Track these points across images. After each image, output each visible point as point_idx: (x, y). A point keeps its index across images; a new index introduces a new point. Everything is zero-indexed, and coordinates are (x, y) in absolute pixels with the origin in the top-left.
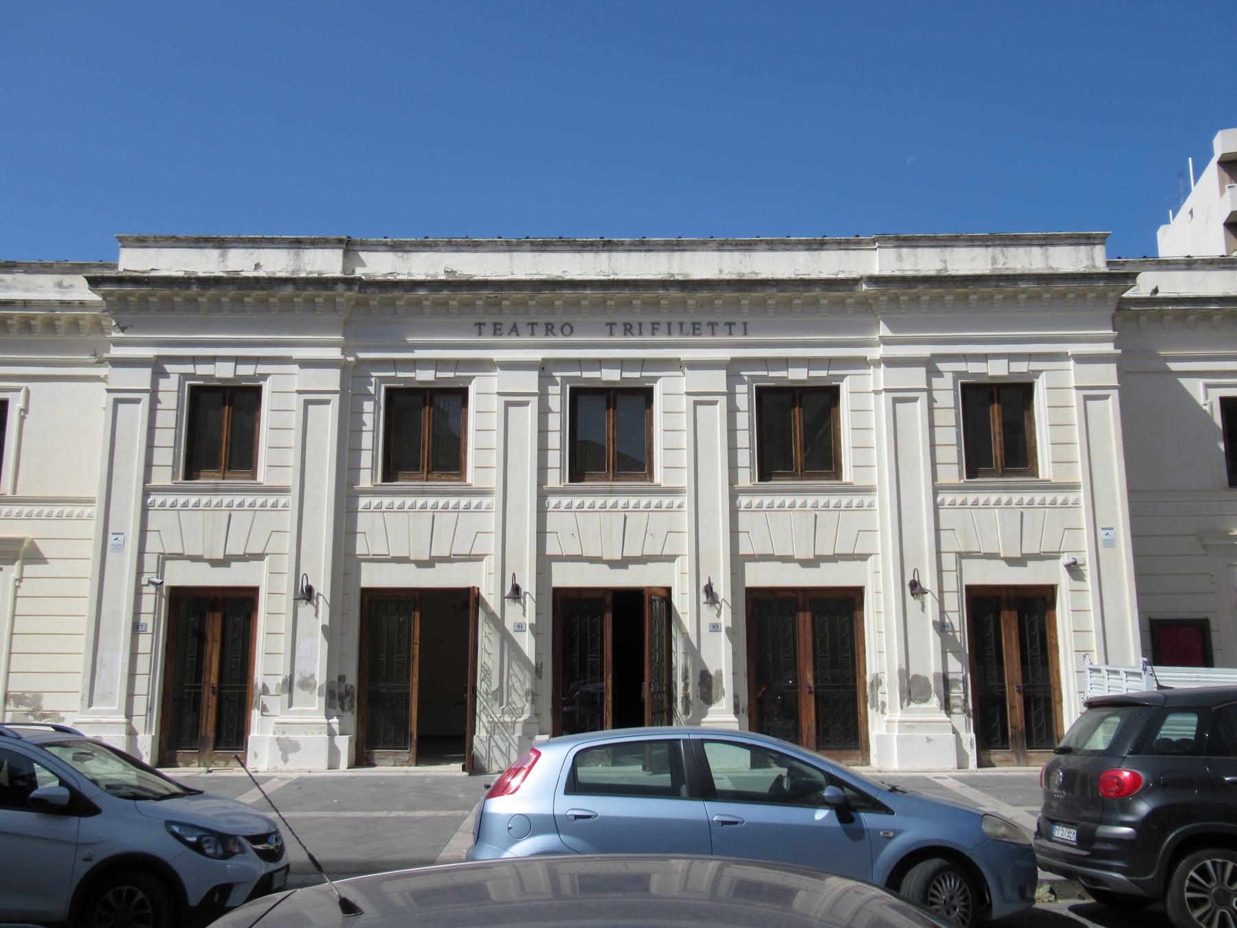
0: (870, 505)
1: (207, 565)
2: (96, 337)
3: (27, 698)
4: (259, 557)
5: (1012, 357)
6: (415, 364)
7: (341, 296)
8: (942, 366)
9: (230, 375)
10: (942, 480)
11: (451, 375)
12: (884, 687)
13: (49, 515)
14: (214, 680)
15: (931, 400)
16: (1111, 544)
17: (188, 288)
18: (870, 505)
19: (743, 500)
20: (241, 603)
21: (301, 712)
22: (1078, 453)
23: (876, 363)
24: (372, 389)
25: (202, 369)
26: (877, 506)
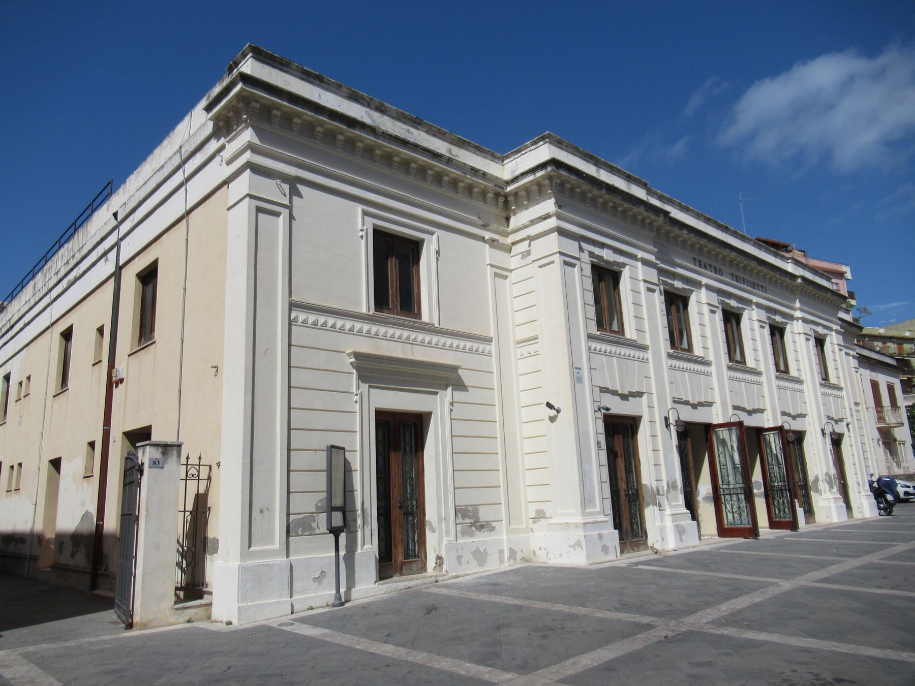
2: (480, 204)
4: (639, 394)
5: (616, 251)
6: (674, 276)
7: (602, 197)
12: (820, 482)
13: (342, 329)
23: (798, 319)
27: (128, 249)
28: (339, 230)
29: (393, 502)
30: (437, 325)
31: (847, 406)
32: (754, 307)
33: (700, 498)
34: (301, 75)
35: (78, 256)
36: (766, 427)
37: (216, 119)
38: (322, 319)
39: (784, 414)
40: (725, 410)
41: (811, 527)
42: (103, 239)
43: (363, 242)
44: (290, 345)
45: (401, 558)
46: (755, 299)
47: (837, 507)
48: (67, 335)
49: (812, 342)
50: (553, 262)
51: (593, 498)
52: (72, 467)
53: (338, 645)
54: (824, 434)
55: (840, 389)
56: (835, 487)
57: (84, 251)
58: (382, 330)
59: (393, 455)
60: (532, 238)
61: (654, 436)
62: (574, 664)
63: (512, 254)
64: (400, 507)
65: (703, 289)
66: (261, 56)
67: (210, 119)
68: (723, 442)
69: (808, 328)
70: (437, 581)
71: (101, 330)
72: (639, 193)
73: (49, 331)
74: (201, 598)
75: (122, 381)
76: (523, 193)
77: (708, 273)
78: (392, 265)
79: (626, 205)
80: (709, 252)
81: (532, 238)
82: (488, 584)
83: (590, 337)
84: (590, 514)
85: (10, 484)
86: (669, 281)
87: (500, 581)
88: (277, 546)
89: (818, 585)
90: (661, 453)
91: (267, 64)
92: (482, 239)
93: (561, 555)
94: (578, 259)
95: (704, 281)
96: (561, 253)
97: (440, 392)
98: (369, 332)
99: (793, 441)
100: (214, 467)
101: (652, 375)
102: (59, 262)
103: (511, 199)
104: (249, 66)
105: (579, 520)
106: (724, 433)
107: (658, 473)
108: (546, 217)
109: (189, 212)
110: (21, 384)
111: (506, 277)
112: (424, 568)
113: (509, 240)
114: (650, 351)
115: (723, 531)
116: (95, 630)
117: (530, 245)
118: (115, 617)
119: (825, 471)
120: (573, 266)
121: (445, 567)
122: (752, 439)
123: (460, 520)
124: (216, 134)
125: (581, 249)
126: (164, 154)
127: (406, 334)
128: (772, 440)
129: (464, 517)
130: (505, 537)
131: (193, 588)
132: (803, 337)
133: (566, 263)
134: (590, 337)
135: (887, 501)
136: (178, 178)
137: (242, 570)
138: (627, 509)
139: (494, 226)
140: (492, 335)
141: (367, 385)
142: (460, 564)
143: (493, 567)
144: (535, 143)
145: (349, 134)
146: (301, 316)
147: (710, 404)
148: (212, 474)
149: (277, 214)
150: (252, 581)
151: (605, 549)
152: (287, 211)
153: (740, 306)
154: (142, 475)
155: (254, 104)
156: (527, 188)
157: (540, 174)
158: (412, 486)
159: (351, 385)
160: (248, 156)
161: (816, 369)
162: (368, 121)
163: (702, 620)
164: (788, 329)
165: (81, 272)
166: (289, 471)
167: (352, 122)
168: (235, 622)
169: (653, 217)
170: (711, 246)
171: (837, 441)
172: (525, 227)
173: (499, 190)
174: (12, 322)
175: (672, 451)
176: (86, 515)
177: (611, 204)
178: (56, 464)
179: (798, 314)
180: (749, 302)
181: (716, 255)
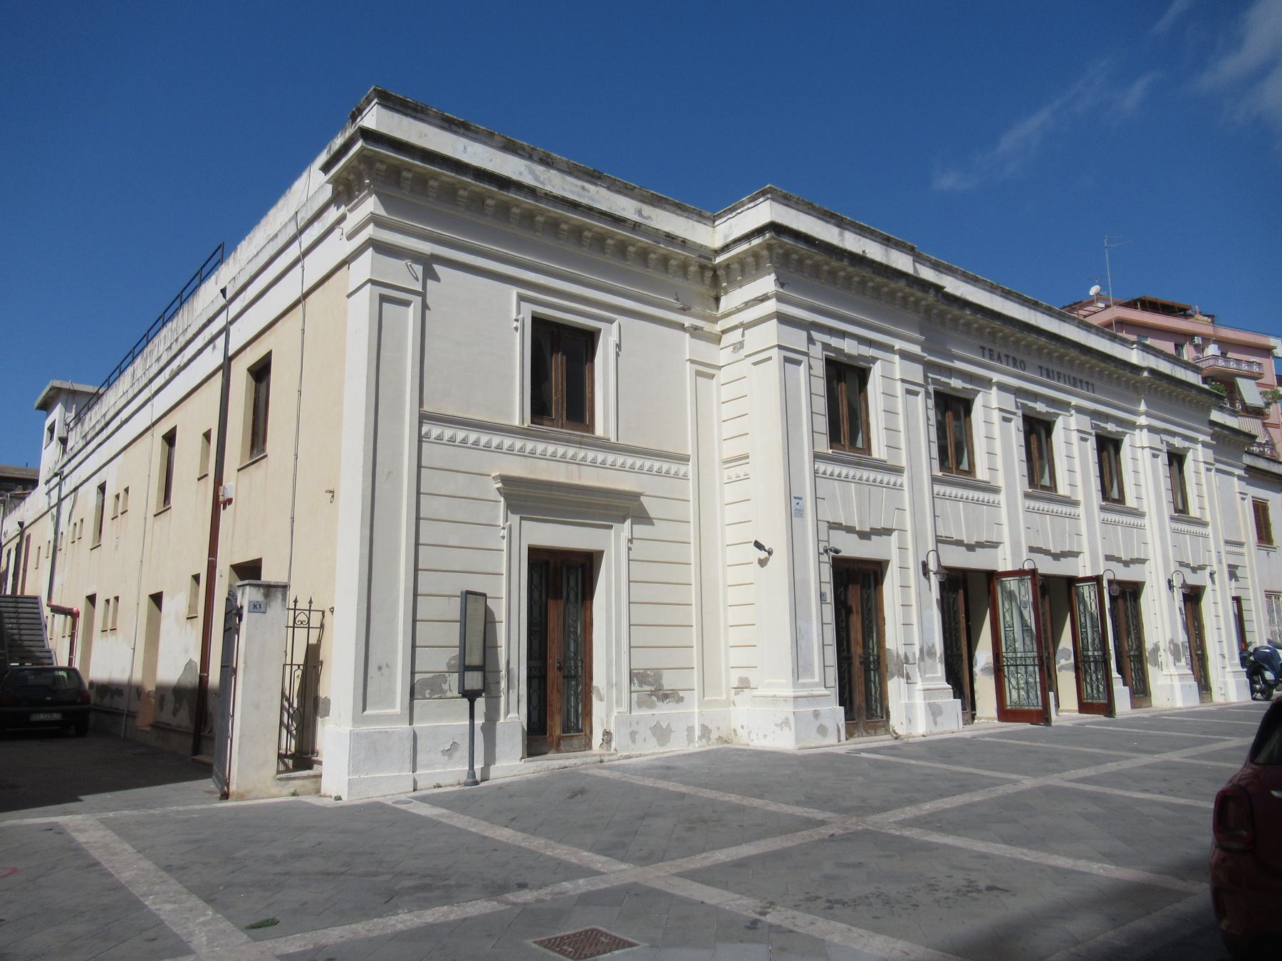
2: (679, 281)
3: (648, 676)
4: (887, 532)
5: (863, 341)
6: (951, 372)
12: (1161, 652)
23: (1141, 427)
27: (240, 334)
28: (486, 322)
29: (550, 661)
30: (613, 440)
31: (1213, 549)
32: (1073, 412)
33: (977, 669)
34: (437, 122)
35: (182, 341)
36: (1081, 576)
37: (335, 181)
38: (461, 434)
39: (1109, 558)
40: (1016, 553)
42: (210, 321)
43: (518, 335)
44: (419, 467)
45: (558, 732)
46: (1074, 401)
47: (1183, 687)
48: (170, 438)
49: (1163, 459)
50: (770, 358)
51: (811, 665)
52: (175, 605)
53: (451, 826)
54: (1171, 587)
55: (1205, 524)
56: (1183, 660)
57: (189, 335)
58: (540, 447)
59: (552, 604)
60: (746, 326)
61: (904, 587)
62: (705, 858)
63: (722, 344)
64: (560, 668)
65: (994, 388)
66: (390, 102)
67: (328, 182)
68: (1011, 596)
69: (1156, 440)
70: (602, 761)
71: (207, 436)
72: (902, 262)
73: (149, 432)
74: (310, 768)
75: (230, 501)
76: (735, 266)
77: (1004, 366)
78: (557, 364)
79: (879, 279)
80: (1005, 338)
81: (746, 326)
82: (662, 767)
83: (817, 457)
84: (804, 685)
85: (105, 623)
86: (943, 379)
87: (677, 764)
88: (398, 710)
89: (1074, 785)
90: (914, 609)
91: (398, 111)
92: (681, 327)
93: (765, 736)
94: (806, 354)
95: (996, 377)
96: (780, 347)
98: (522, 449)
99: (1129, 593)
100: (328, 613)
101: (907, 506)
102: (161, 346)
103: (721, 273)
104: (374, 118)
105: (790, 692)
106: (1012, 584)
107: (908, 634)
108: (764, 299)
109: (305, 296)
110: (118, 497)
111: (712, 376)
112: (588, 745)
113: (718, 327)
114: (905, 474)
115: (1005, 714)
116: (186, 800)
117: (743, 335)
118: (213, 786)
119: (1169, 637)
120: (798, 363)
121: (613, 744)
122: (1056, 594)
123: (635, 687)
124: (336, 200)
125: (811, 340)
126: (278, 219)
127: (571, 451)
128: (1086, 594)
129: (641, 683)
130: (697, 710)
131: (302, 757)
132: (1148, 452)
133: (787, 360)
135: (1265, 681)
136: (293, 252)
137: (354, 736)
138: (862, 680)
139: (697, 309)
140: (690, 452)
141: (517, 517)
142: (634, 741)
143: (678, 746)
144: (753, 199)
145: (500, 197)
146: (435, 430)
147: (995, 545)
148: (326, 622)
149: (406, 304)
150: (366, 750)
151: (822, 730)
152: (420, 299)
153: (1052, 410)
154: (240, 620)
155: (378, 165)
156: (741, 260)
157: (756, 241)
158: (576, 641)
159: (497, 517)
160: (370, 231)
161: (1166, 496)
162: (527, 180)
163: (887, 821)
164: (1126, 441)
165: (185, 360)
166: (414, 621)
167: (504, 183)
168: (345, 798)
169: (920, 294)
170: (1007, 330)
171: (1193, 597)
172: (738, 310)
173: (706, 262)
174: (107, 418)
175: (930, 607)
176: (190, 664)
177: (856, 279)
178: (157, 599)
179: (1142, 420)
180: (1065, 406)
181: (1017, 342)
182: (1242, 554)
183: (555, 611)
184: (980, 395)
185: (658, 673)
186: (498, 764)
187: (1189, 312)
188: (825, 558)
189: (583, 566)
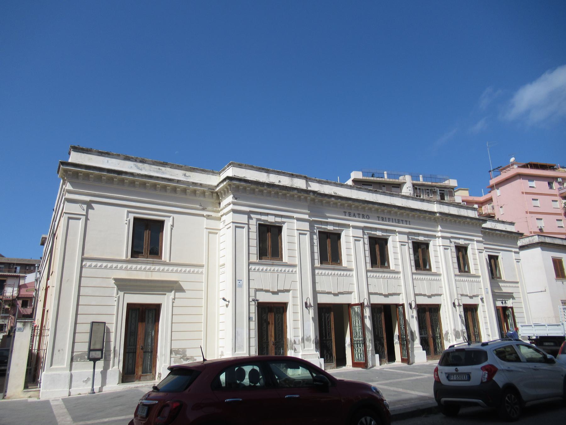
0: (295, 272)
1: (271, 294)
2: (202, 199)
4: (288, 291)
5: (465, 239)
6: (327, 223)
8: (252, 216)
9: (273, 221)
10: (251, 260)
11: (337, 228)
12: (449, 335)
13: (189, 272)
14: (273, 339)
15: (249, 228)
16: (241, 286)
17: (263, 187)
18: (295, 272)
19: (317, 271)
20: (281, 308)
21: (308, 350)
22: (297, 254)
23: (439, 237)
24: (315, 231)
25: (263, 218)
26: (442, 280)
28: (113, 224)
29: (138, 346)
30: (168, 261)
41: (30, 396)
43: (127, 226)
45: (140, 373)
64: (142, 349)
66: (77, 149)
72: (300, 183)
83: (456, 275)
88: (65, 366)
92: (203, 216)
96: (233, 222)
97: (167, 294)
119: (453, 328)
125: (451, 242)
134: (456, 275)
141: (123, 293)
144: (228, 166)
146: (88, 263)
147: (350, 293)
155: (69, 173)
157: (225, 183)
179: (439, 234)
182: (518, 287)
183: (141, 328)
184: (344, 231)
185: (184, 351)
186: (107, 386)
187: (555, 167)
188: (253, 303)
189: (155, 309)
